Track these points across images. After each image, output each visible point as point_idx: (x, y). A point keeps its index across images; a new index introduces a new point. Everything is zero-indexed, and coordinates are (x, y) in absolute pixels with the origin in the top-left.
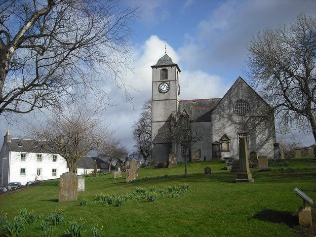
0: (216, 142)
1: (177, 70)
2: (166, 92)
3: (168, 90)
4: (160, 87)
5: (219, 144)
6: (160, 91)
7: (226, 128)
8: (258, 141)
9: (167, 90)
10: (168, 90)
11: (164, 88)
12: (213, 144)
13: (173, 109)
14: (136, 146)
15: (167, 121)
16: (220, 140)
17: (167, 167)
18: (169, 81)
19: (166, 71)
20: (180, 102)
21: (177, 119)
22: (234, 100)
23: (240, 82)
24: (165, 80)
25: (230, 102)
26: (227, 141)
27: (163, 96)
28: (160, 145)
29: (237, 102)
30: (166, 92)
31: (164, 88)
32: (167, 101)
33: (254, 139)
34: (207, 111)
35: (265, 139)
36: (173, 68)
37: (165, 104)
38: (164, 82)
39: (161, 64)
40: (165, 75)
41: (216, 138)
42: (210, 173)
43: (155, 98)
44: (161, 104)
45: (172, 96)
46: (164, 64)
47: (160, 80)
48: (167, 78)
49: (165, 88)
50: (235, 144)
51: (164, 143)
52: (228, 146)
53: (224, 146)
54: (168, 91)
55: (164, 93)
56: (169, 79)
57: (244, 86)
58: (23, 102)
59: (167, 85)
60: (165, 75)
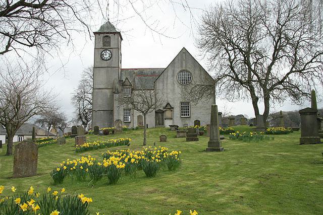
3: (111, 58)
27: (105, 64)
30: (109, 59)
37: (107, 71)
38: (106, 50)
43: (98, 65)
44: (103, 71)
55: (106, 60)
59: (109, 52)
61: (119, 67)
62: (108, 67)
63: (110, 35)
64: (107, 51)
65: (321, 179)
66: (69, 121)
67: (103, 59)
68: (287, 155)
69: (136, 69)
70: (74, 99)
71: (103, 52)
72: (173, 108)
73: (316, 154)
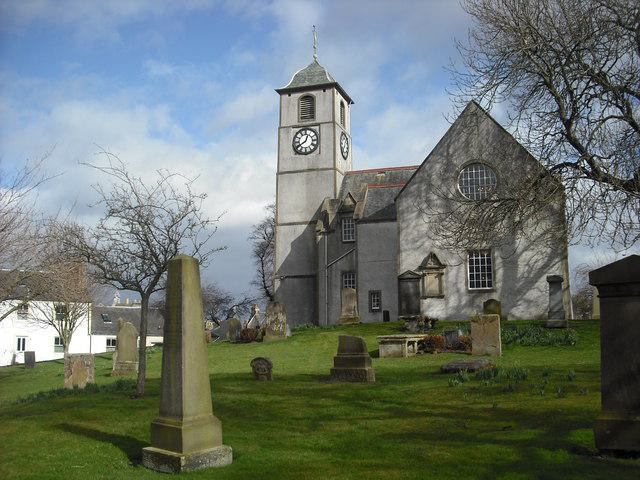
0: (409, 272)
1: (339, 98)
2: (312, 151)
3: (316, 147)
4: (297, 140)
5: (416, 278)
6: (297, 150)
7: (420, 236)
8: (522, 269)
9: (312, 147)
10: (316, 147)
11: (307, 142)
12: (401, 279)
13: (326, 193)
14: (254, 283)
15: (311, 223)
16: (421, 268)
17: (261, 340)
18: (319, 124)
19: (311, 99)
20: (348, 175)
21: (331, 218)
22: (459, 161)
23: (473, 114)
24: (307, 123)
25: (448, 166)
26: (437, 269)
27: (303, 162)
28: (296, 280)
29: (465, 167)
30: (312, 151)
31: (307, 142)
32: (311, 173)
33: (511, 262)
34: (393, 193)
35: (540, 264)
36: (329, 92)
37: (308, 181)
38: (306, 128)
39: (301, 85)
40: (308, 110)
41: (410, 261)
42: (269, 376)
43: (286, 167)
44: (299, 179)
45: (324, 162)
46: (307, 84)
47: (297, 124)
48: (313, 117)
49: (309, 141)
50: (458, 274)
51: (301, 277)
52: (440, 282)
53: (430, 282)
54: (315, 149)
55: (306, 154)
56: (319, 118)
57: (485, 125)
58: (305, 167)
59: (312, 134)
60: (308, 110)
61: (335, 169)
62: (309, 170)
63: (313, 93)
64: (308, 132)
65: (501, 2)
66: (237, 302)
67: (298, 153)
68: (171, 456)
69: (381, 171)
70: (141, 218)
71: (299, 135)
72: (444, 266)
73: (367, 414)
